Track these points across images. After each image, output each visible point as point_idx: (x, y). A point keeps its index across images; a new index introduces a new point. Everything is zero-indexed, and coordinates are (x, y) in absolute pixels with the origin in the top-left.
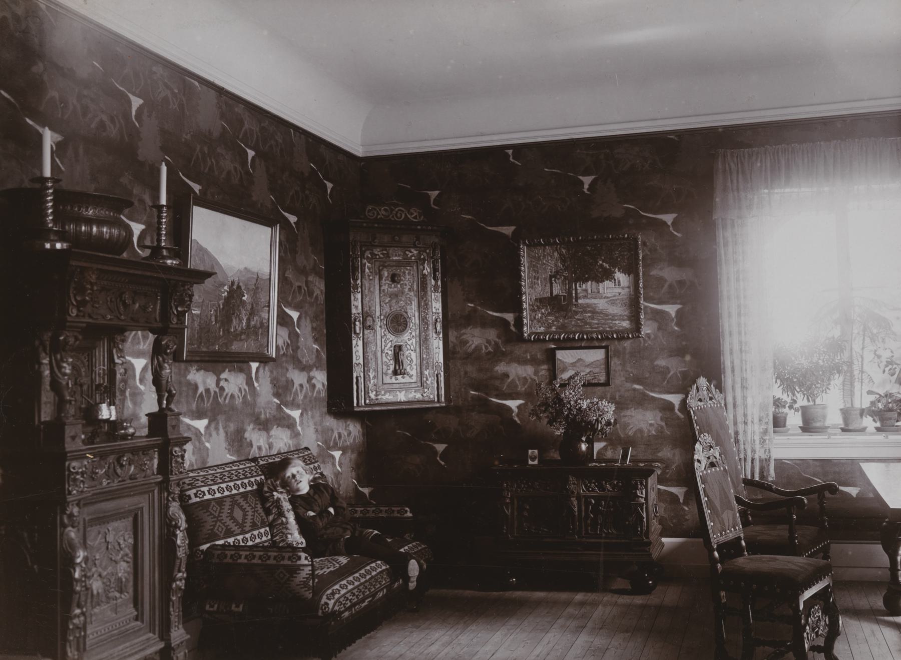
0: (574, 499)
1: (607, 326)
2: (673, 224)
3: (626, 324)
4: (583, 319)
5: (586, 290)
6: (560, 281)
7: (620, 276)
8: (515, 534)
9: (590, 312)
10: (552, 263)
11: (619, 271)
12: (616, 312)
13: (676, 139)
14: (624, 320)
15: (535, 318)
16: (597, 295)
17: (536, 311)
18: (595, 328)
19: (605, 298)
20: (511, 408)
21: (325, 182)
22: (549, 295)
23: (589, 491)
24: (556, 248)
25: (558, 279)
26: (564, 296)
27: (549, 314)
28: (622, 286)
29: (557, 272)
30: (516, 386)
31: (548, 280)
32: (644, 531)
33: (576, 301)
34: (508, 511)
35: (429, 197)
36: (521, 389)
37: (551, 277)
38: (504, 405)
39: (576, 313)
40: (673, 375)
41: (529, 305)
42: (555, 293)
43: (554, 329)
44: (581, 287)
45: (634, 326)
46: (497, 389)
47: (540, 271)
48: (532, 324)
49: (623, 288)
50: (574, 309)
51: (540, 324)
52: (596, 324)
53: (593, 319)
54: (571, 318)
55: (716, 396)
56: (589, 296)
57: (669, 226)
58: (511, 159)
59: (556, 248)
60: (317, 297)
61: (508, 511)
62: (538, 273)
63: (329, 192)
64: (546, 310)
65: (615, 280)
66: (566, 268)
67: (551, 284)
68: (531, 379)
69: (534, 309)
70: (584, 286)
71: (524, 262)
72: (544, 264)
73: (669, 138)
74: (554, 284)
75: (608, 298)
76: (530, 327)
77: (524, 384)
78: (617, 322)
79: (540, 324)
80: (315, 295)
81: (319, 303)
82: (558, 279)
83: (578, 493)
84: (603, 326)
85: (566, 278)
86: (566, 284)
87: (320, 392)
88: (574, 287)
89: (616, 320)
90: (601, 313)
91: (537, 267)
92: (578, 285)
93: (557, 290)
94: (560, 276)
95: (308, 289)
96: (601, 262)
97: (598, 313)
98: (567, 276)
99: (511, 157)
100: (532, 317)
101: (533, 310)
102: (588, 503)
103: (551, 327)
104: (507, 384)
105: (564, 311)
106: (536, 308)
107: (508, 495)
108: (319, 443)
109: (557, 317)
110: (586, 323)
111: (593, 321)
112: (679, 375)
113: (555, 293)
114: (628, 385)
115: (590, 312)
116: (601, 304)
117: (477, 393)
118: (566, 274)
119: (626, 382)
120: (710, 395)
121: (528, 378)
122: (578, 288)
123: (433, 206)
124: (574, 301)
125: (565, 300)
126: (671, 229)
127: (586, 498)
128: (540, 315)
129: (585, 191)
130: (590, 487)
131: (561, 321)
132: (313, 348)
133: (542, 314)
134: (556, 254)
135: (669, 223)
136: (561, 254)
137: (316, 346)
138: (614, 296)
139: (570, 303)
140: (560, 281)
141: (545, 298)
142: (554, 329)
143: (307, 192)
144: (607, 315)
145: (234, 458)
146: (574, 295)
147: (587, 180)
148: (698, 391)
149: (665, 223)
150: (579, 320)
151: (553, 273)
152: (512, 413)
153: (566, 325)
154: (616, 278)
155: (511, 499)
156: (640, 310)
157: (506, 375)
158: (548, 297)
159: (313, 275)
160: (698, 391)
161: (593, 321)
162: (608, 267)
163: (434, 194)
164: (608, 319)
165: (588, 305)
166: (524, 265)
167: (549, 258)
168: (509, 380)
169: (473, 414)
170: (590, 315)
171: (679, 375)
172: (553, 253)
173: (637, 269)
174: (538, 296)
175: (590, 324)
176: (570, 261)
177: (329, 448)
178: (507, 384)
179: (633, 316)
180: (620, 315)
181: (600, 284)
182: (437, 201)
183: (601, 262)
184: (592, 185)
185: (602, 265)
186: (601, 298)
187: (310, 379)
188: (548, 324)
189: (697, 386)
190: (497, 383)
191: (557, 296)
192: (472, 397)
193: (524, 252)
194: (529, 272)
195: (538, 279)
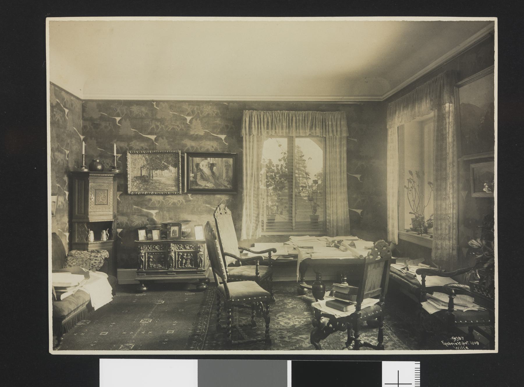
1: (165, 189)
3: (174, 188)
4: (155, 186)
6: (145, 169)
7: (171, 168)
8: (146, 269)
12: (169, 183)
13: (227, 104)
14: (173, 187)
15: (133, 185)
19: (165, 177)
20: (152, 214)
21: (64, 109)
22: (140, 175)
23: (179, 250)
24: (144, 155)
25: (144, 168)
26: (147, 176)
27: (140, 183)
30: (155, 204)
31: (140, 168)
32: (203, 266)
33: (152, 178)
35: (116, 120)
37: (141, 167)
38: (149, 212)
41: (131, 179)
42: (143, 174)
43: (142, 190)
44: (155, 172)
45: (177, 189)
46: (146, 205)
47: (136, 165)
48: (132, 187)
49: (173, 173)
50: (151, 181)
51: (136, 187)
52: (161, 188)
53: (160, 186)
54: (150, 185)
55: (228, 212)
56: (158, 176)
57: (223, 140)
58: (155, 106)
59: (144, 155)
60: (59, 162)
62: (135, 165)
63: (66, 113)
64: (139, 181)
65: (169, 170)
66: (148, 164)
67: (141, 171)
71: (129, 160)
72: (138, 162)
75: (166, 177)
77: (159, 203)
78: (170, 187)
79: (136, 187)
80: (58, 161)
81: (60, 165)
83: (175, 251)
84: (164, 189)
85: (148, 168)
86: (148, 171)
87: (60, 206)
88: (151, 172)
89: (169, 187)
90: (163, 183)
91: (135, 163)
92: (153, 171)
93: (144, 173)
94: (145, 167)
95: (54, 159)
96: (163, 162)
97: (162, 183)
98: (149, 168)
99: (155, 105)
101: (133, 182)
102: (178, 255)
103: (141, 189)
104: (151, 203)
105: (147, 182)
106: (134, 181)
107: (143, 252)
109: (143, 185)
110: (157, 188)
111: (160, 187)
112: (225, 201)
113: (143, 174)
116: (163, 180)
119: (204, 203)
122: (153, 172)
123: (118, 124)
124: (151, 178)
128: (136, 184)
129: (188, 123)
131: (145, 186)
132: (57, 186)
133: (137, 183)
135: (223, 139)
136: (146, 158)
137: (58, 185)
138: (169, 177)
139: (150, 179)
140: (145, 169)
142: (142, 190)
143: (55, 113)
144: (166, 184)
145: (460, 104)
146: (151, 176)
148: (220, 210)
149: (221, 139)
150: (153, 186)
151: (142, 166)
153: (148, 188)
154: (170, 169)
155: (145, 254)
160: (220, 210)
161: (160, 187)
162: (166, 164)
164: (166, 186)
166: (129, 162)
169: (135, 216)
170: (158, 184)
171: (225, 201)
172: (142, 157)
173: (179, 166)
174: (135, 176)
175: (158, 188)
179: (177, 185)
181: (163, 171)
182: (120, 122)
183: (163, 162)
184: (191, 121)
185: (164, 163)
188: (139, 188)
189: (220, 208)
190: (146, 203)
191: (144, 176)
192: (134, 209)
193: (129, 156)
194: (131, 165)
195: (135, 168)
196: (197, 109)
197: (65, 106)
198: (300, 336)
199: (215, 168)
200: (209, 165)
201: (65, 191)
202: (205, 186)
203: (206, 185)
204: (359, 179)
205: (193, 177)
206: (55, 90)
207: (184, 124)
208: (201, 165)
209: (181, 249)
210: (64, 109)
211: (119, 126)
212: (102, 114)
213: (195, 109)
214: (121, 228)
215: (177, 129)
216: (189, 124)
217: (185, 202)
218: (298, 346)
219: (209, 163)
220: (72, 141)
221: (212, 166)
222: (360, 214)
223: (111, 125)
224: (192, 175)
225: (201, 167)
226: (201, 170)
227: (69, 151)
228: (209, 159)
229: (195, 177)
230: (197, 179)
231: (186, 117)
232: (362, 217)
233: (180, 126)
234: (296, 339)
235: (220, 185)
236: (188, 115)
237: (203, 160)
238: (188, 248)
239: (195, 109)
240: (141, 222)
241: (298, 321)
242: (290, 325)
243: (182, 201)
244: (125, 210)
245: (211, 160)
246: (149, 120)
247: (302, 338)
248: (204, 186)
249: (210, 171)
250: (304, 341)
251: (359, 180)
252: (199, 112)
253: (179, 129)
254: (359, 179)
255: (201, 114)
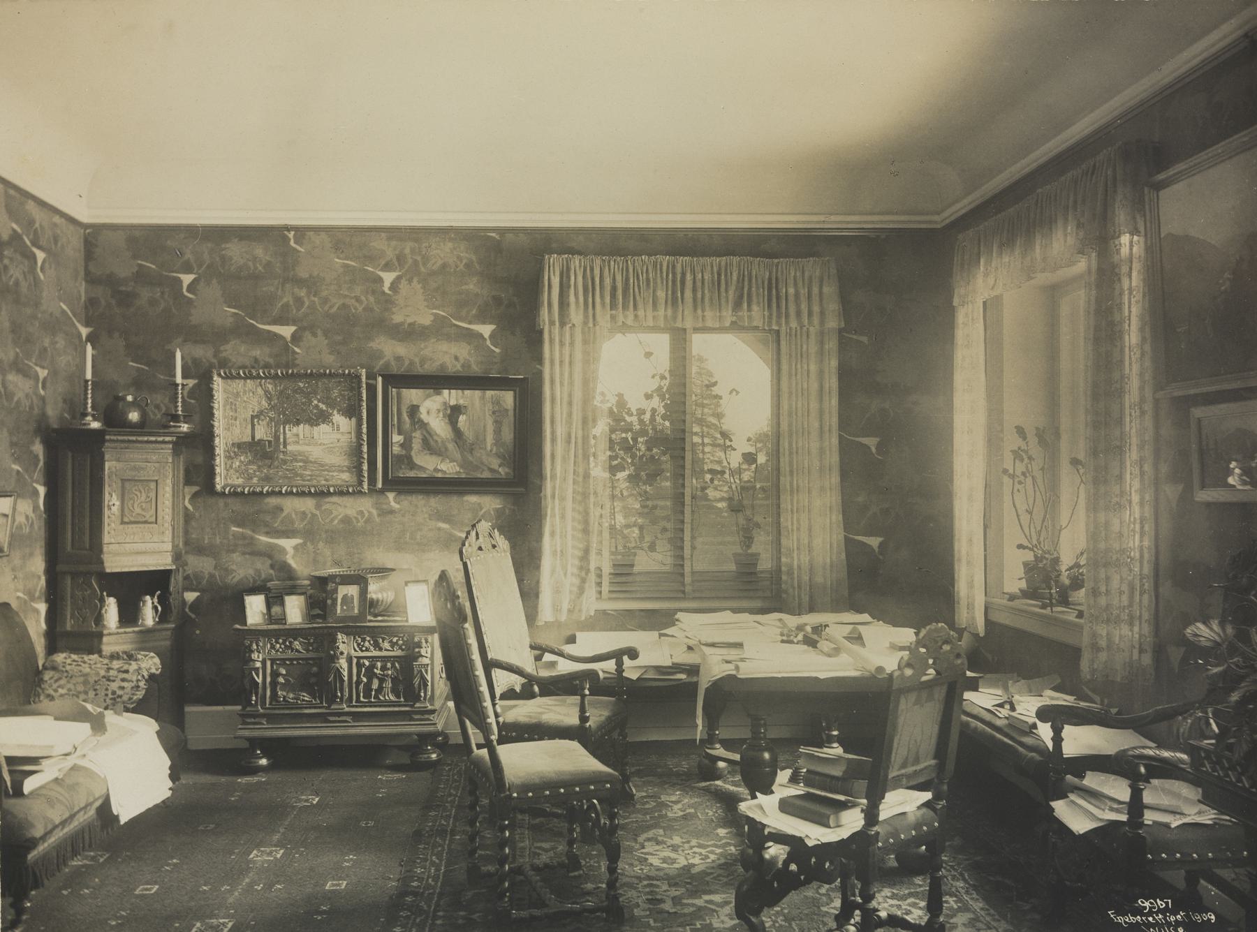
0: (345, 660)
1: (322, 478)
2: (491, 337)
3: (346, 476)
5: (297, 435)
6: (265, 422)
7: (338, 418)
9: (301, 461)
10: (254, 401)
11: (339, 413)
12: (333, 461)
14: (343, 472)
16: (311, 441)
17: (233, 458)
18: (308, 480)
21: (35, 250)
22: (249, 439)
23: (362, 651)
26: (270, 442)
27: (250, 462)
28: (341, 430)
29: (261, 412)
30: (292, 522)
34: (258, 677)
35: (180, 281)
36: (299, 525)
38: (276, 545)
39: (285, 462)
40: (485, 512)
41: (225, 451)
42: (257, 437)
44: (292, 432)
45: (355, 479)
46: (266, 525)
53: (305, 469)
54: (277, 467)
56: (301, 442)
57: (486, 339)
58: (292, 243)
60: (18, 402)
61: (258, 677)
62: (236, 411)
63: (39, 264)
64: (247, 457)
65: (333, 424)
68: (312, 513)
69: (230, 456)
70: (295, 430)
73: (489, 236)
74: (256, 427)
76: (226, 478)
77: (302, 520)
78: (335, 474)
80: (16, 399)
82: (263, 420)
85: (271, 419)
88: (282, 431)
90: (315, 462)
93: (262, 433)
96: (316, 402)
97: (311, 462)
100: (228, 466)
101: (229, 457)
102: (359, 666)
103: (251, 478)
106: (232, 454)
107: (258, 657)
108: (20, 594)
109: (259, 467)
110: (297, 475)
112: (492, 513)
113: (257, 437)
114: (433, 524)
115: (301, 461)
117: (241, 530)
118: (272, 414)
120: (493, 543)
121: (307, 512)
122: (287, 432)
124: (281, 447)
125: (270, 445)
126: (488, 343)
127: (359, 658)
130: (363, 646)
131: (265, 471)
132: (13, 469)
133: (241, 461)
134: (260, 391)
135: (486, 335)
136: (266, 391)
137: (16, 467)
139: (277, 449)
140: (265, 422)
141: (245, 443)
142: (255, 480)
144: (322, 466)
145: (1162, 236)
147: (388, 277)
149: (481, 336)
152: (286, 555)
154: (334, 421)
156: (362, 460)
157: (280, 509)
158: (249, 443)
159: (14, 372)
160: (477, 538)
162: (324, 408)
163: (187, 279)
164: (324, 471)
165: (300, 453)
167: (251, 394)
168: (284, 514)
170: (301, 464)
174: (236, 441)
175: (301, 476)
176: (278, 399)
177: (32, 598)
178: (280, 519)
180: (339, 466)
182: (191, 288)
183: (316, 402)
185: (317, 406)
186: (316, 444)
187: (496, 363)
190: (268, 518)
193: (218, 385)
195: (236, 420)
196: (413, 251)
197: (35, 244)
198: (707, 897)
199: (462, 418)
200: (446, 409)
201: (35, 485)
202: (436, 470)
203: (439, 467)
204: (874, 450)
205: (402, 445)
206: (7, 195)
207: (373, 292)
208: (423, 410)
209: (367, 650)
210: (35, 250)
211: (191, 299)
212: (140, 266)
213: (407, 251)
214: (194, 590)
215: (356, 309)
216: (389, 295)
217: (379, 515)
218: (699, 926)
219: (445, 403)
220: (56, 343)
221: (453, 413)
222: (877, 550)
223: (166, 296)
224: (396, 438)
225: (423, 416)
226: (424, 425)
227: (46, 372)
228: (446, 392)
229: (406, 445)
230: (411, 448)
231: (381, 274)
232: (881, 557)
233: (363, 298)
234: (693, 905)
235: (477, 468)
236: (388, 267)
237: (428, 396)
238: (386, 645)
239: (407, 251)
240: (251, 572)
241: (701, 854)
242: (676, 866)
243: (369, 512)
244: (206, 537)
245: (452, 396)
246: (276, 282)
247: (710, 902)
248: (432, 469)
249: (449, 428)
250: (717, 912)
251: (872, 454)
252: (419, 258)
253: (360, 309)
254: (874, 450)
255: (424, 264)
